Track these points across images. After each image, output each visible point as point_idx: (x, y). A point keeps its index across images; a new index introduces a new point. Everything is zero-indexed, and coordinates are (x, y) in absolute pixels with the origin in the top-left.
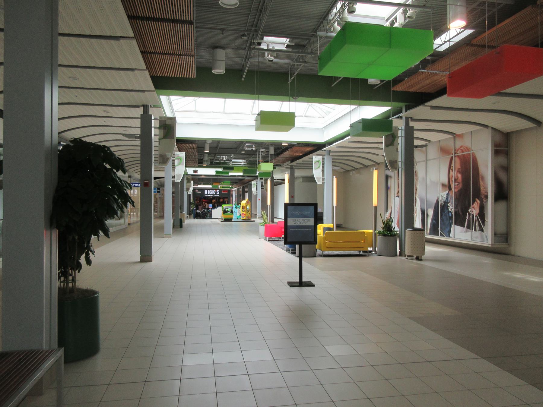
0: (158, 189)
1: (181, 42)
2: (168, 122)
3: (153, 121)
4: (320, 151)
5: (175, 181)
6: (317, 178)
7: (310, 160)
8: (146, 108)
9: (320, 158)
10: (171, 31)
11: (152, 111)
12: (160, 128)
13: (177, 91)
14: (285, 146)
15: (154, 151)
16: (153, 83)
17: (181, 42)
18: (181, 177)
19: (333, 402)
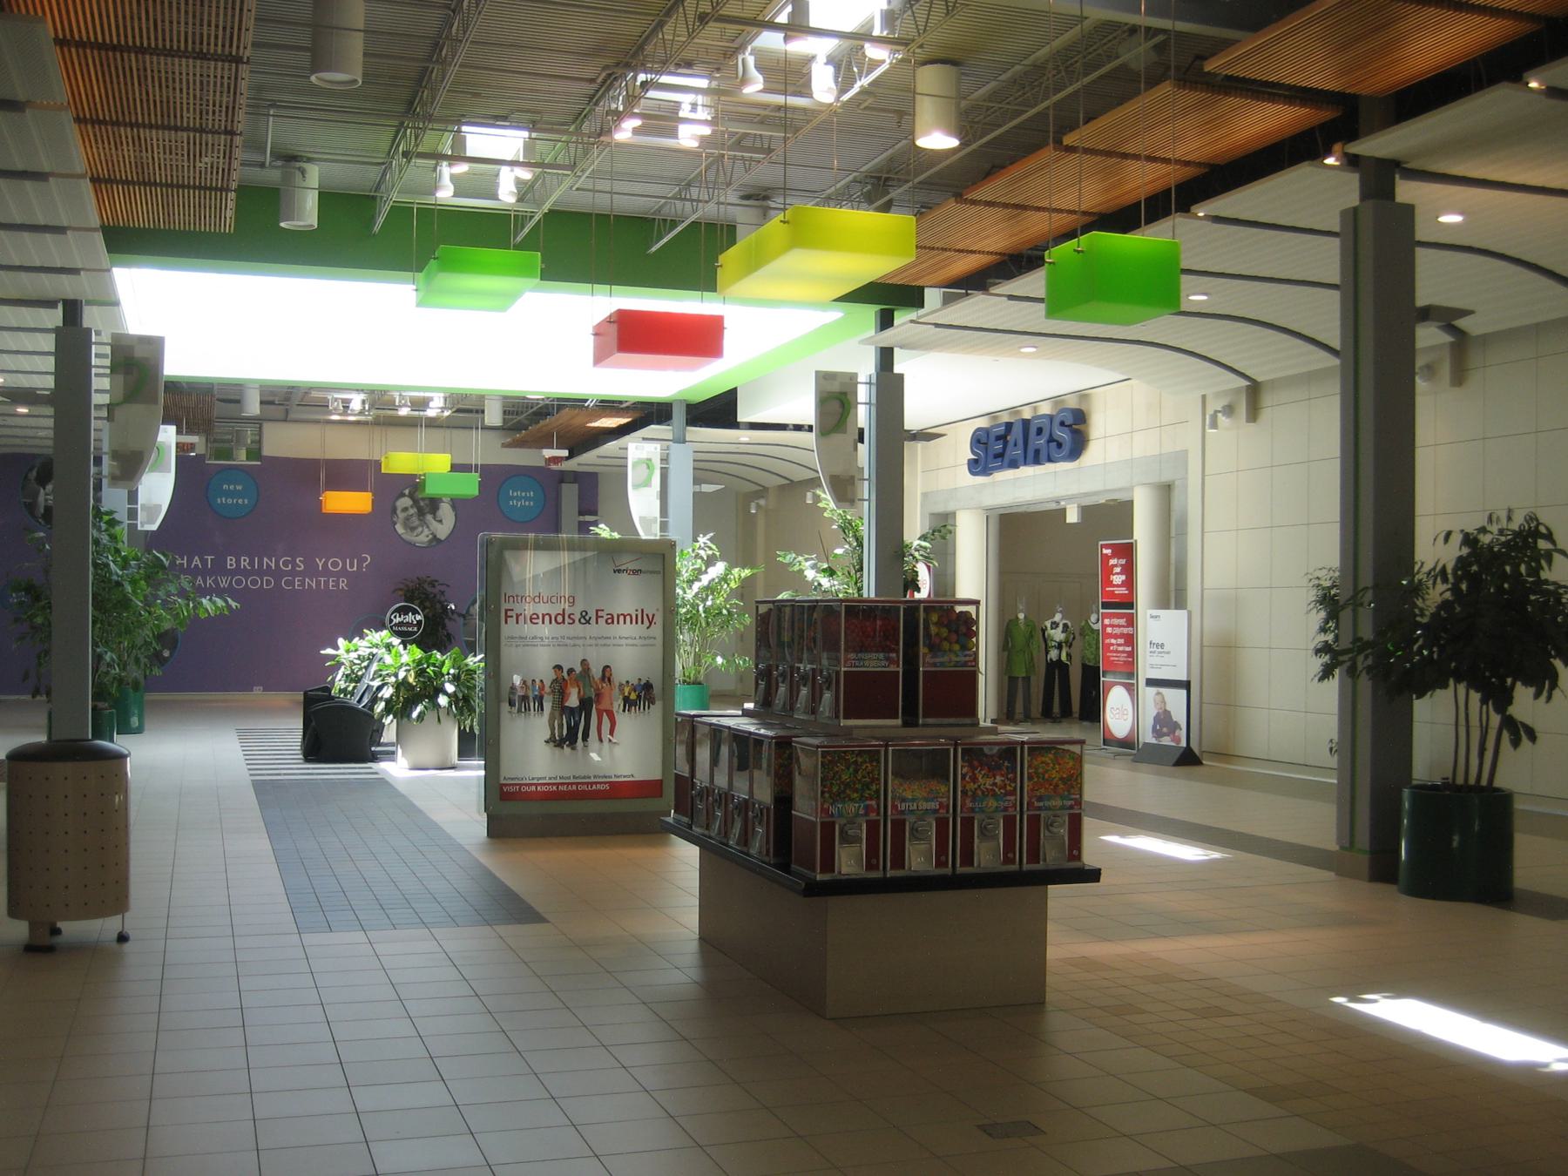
0: (899, 122)
1: (86, 23)
2: (139, 353)
3: (93, 347)
4: (652, 426)
5: (139, 528)
6: (642, 519)
7: (621, 453)
8: (73, 310)
9: (653, 450)
10: (108, 17)
11: (91, 317)
12: (114, 368)
13: (144, 257)
14: (498, 119)
15: (95, 430)
16: (1414, 464)
17: (86, 23)
18: (158, 516)
19: (596, 1155)
